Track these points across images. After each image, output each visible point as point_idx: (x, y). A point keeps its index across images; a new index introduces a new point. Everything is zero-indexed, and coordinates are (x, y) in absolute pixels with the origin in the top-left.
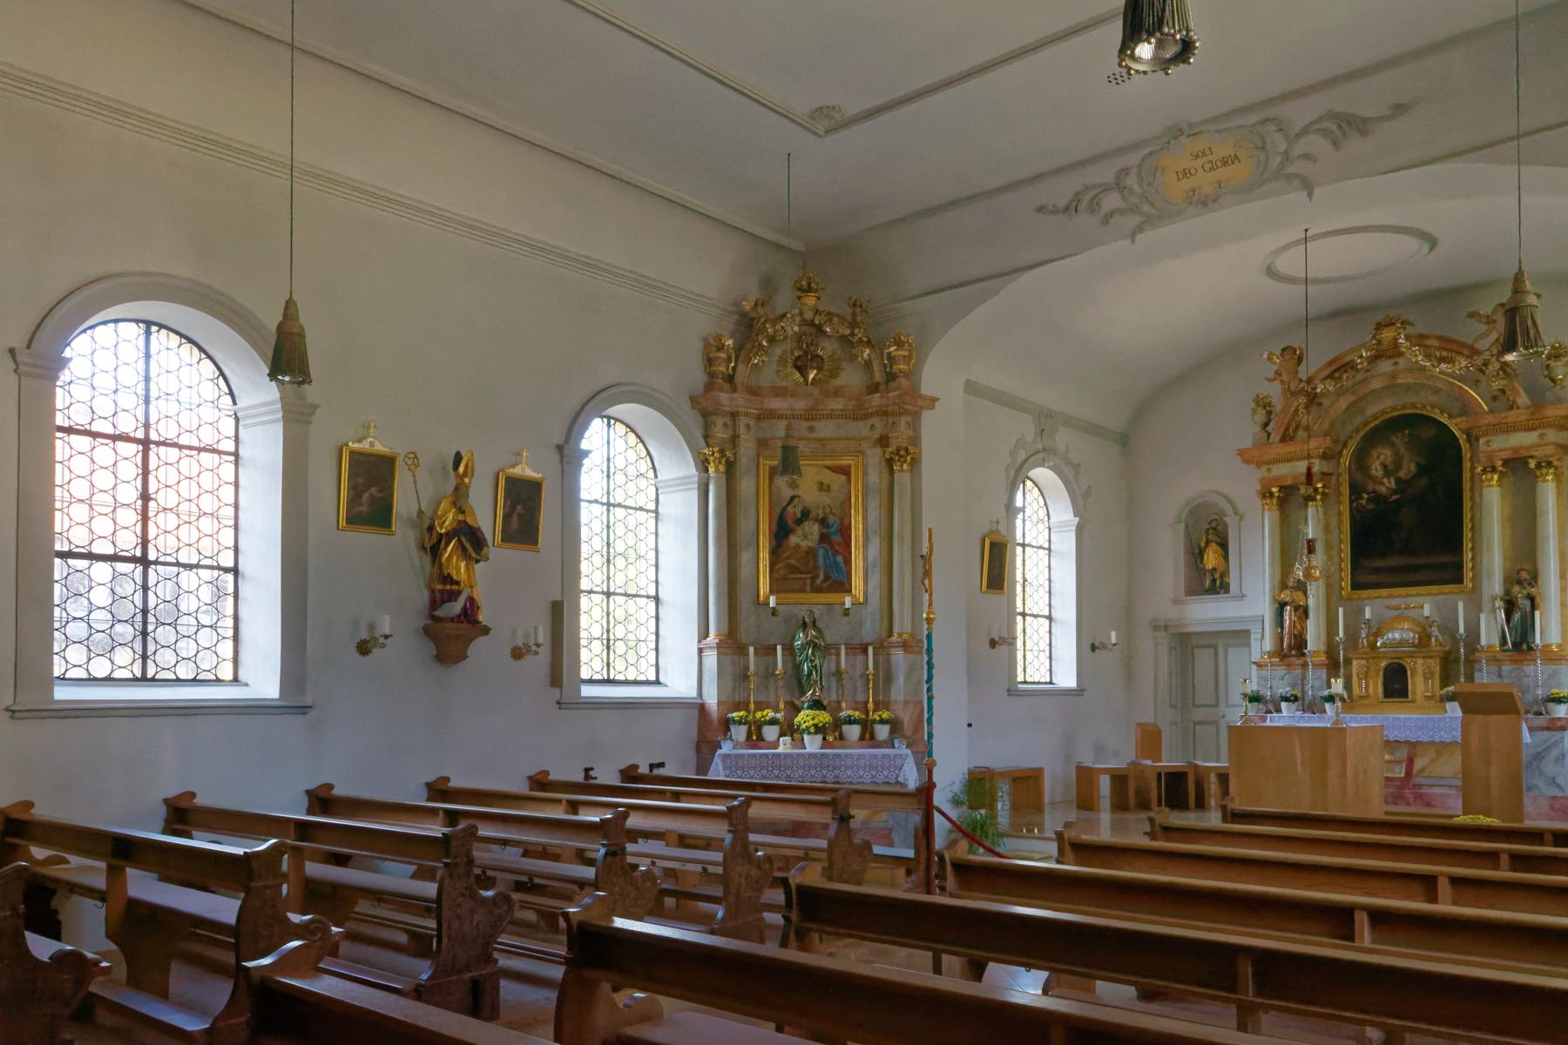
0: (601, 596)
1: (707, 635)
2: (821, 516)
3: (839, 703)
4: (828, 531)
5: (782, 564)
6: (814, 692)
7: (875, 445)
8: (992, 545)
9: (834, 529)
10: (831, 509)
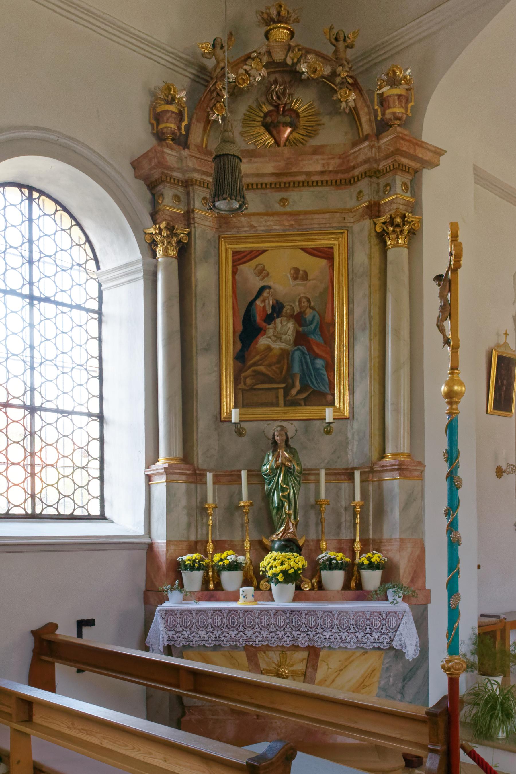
0: (22, 411)
1: (156, 460)
2: (297, 310)
3: (318, 541)
4: (305, 328)
5: (249, 372)
6: (287, 528)
7: (362, 217)
8: (500, 359)
9: (313, 326)
10: (309, 301)
